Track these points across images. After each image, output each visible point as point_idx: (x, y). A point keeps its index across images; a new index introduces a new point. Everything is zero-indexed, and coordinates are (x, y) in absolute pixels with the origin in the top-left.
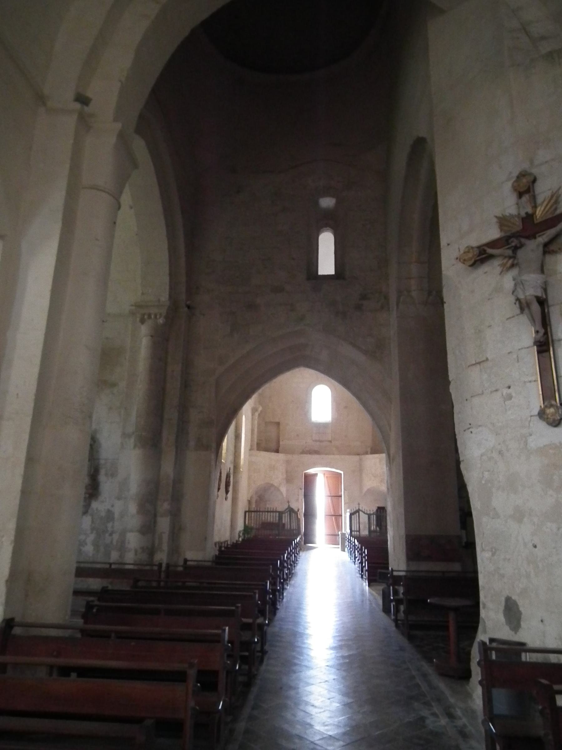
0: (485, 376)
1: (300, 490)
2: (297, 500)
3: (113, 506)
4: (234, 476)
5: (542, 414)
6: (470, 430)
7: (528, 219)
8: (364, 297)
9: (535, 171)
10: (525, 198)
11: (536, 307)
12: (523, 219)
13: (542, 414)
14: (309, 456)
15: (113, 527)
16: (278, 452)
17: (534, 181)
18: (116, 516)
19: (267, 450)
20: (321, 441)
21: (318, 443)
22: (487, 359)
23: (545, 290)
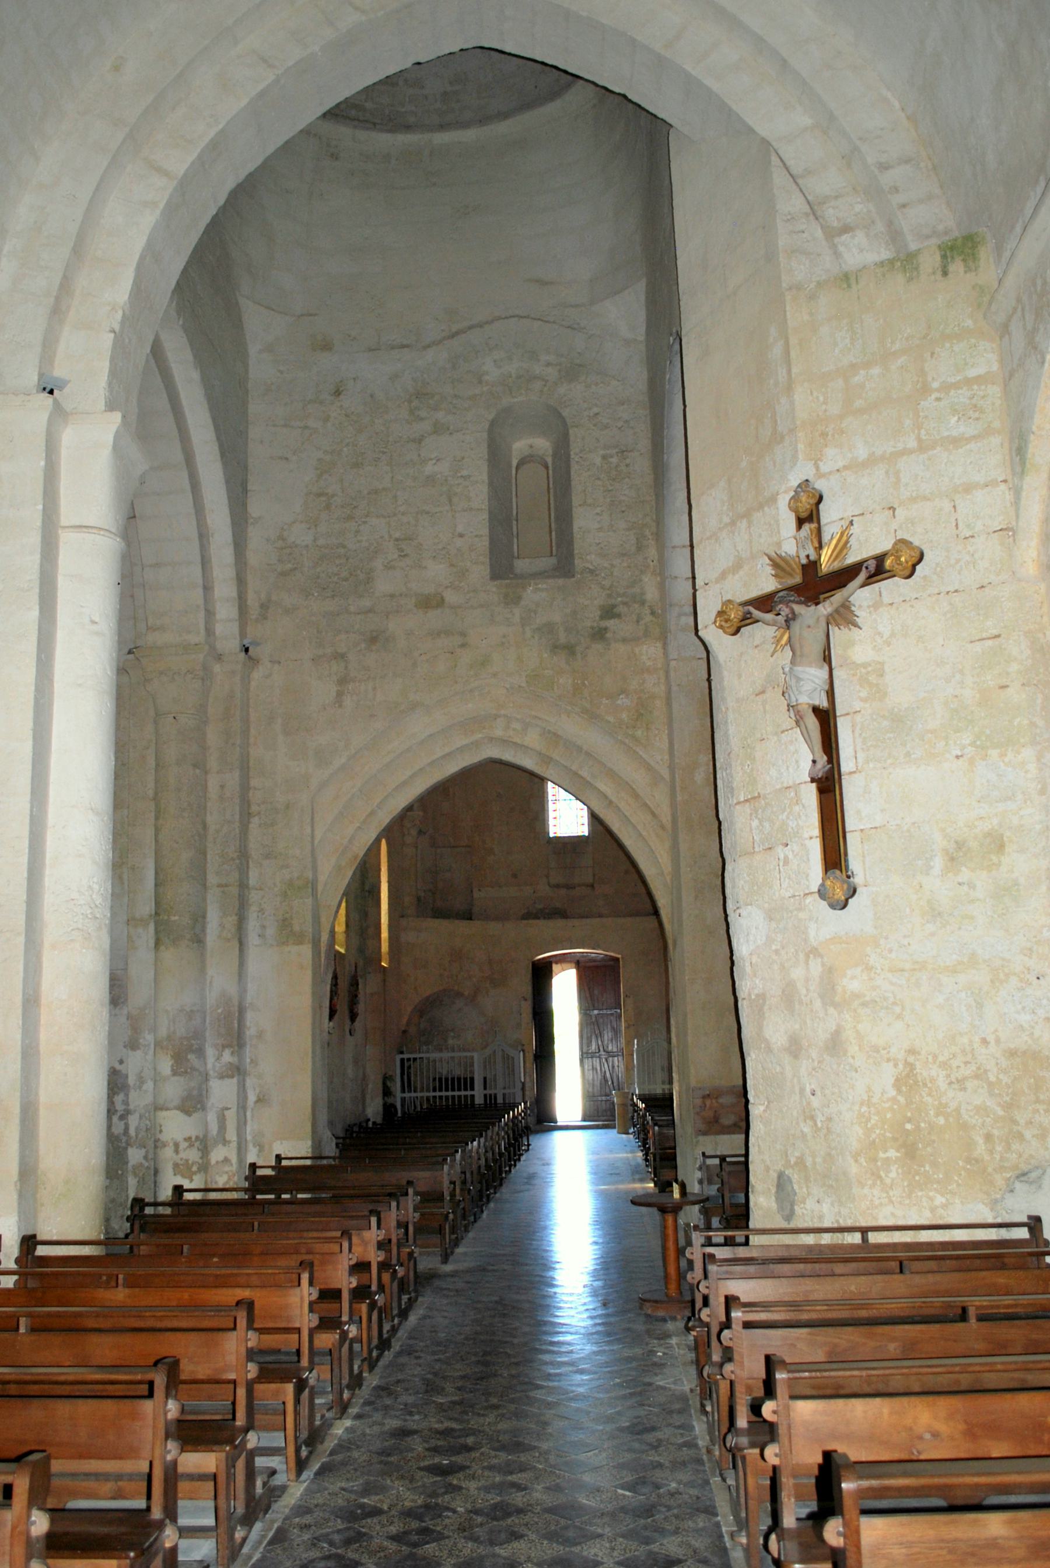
0: (755, 823)
1: (523, 1002)
2: (519, 1025)
3: (121, 1062)
4: (90, 1457)
5: (822, 893)
6: (738, 911)
7: (811, 567)
8: (609, 612)
9: (820, 485)
10: (807, 527)
11: (813, 723)
12: (804, 567)
13: (822, 893)
14: (541, 923)
15: (126, 1103)
16: (471, 919)
17: (821, 499)
18: (131, 1080)
19: (440, 914)
20: (569, 887)
21: (563, 892)
22: (759, 796)
23: (831, 694)
